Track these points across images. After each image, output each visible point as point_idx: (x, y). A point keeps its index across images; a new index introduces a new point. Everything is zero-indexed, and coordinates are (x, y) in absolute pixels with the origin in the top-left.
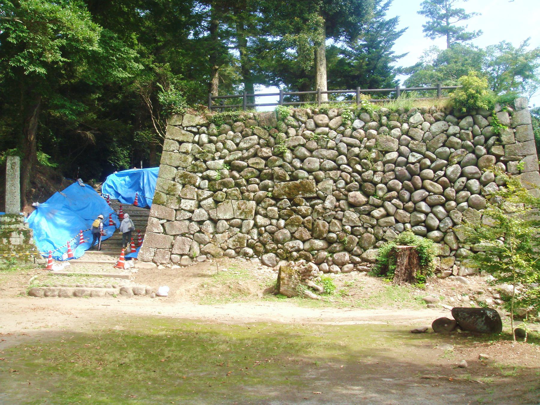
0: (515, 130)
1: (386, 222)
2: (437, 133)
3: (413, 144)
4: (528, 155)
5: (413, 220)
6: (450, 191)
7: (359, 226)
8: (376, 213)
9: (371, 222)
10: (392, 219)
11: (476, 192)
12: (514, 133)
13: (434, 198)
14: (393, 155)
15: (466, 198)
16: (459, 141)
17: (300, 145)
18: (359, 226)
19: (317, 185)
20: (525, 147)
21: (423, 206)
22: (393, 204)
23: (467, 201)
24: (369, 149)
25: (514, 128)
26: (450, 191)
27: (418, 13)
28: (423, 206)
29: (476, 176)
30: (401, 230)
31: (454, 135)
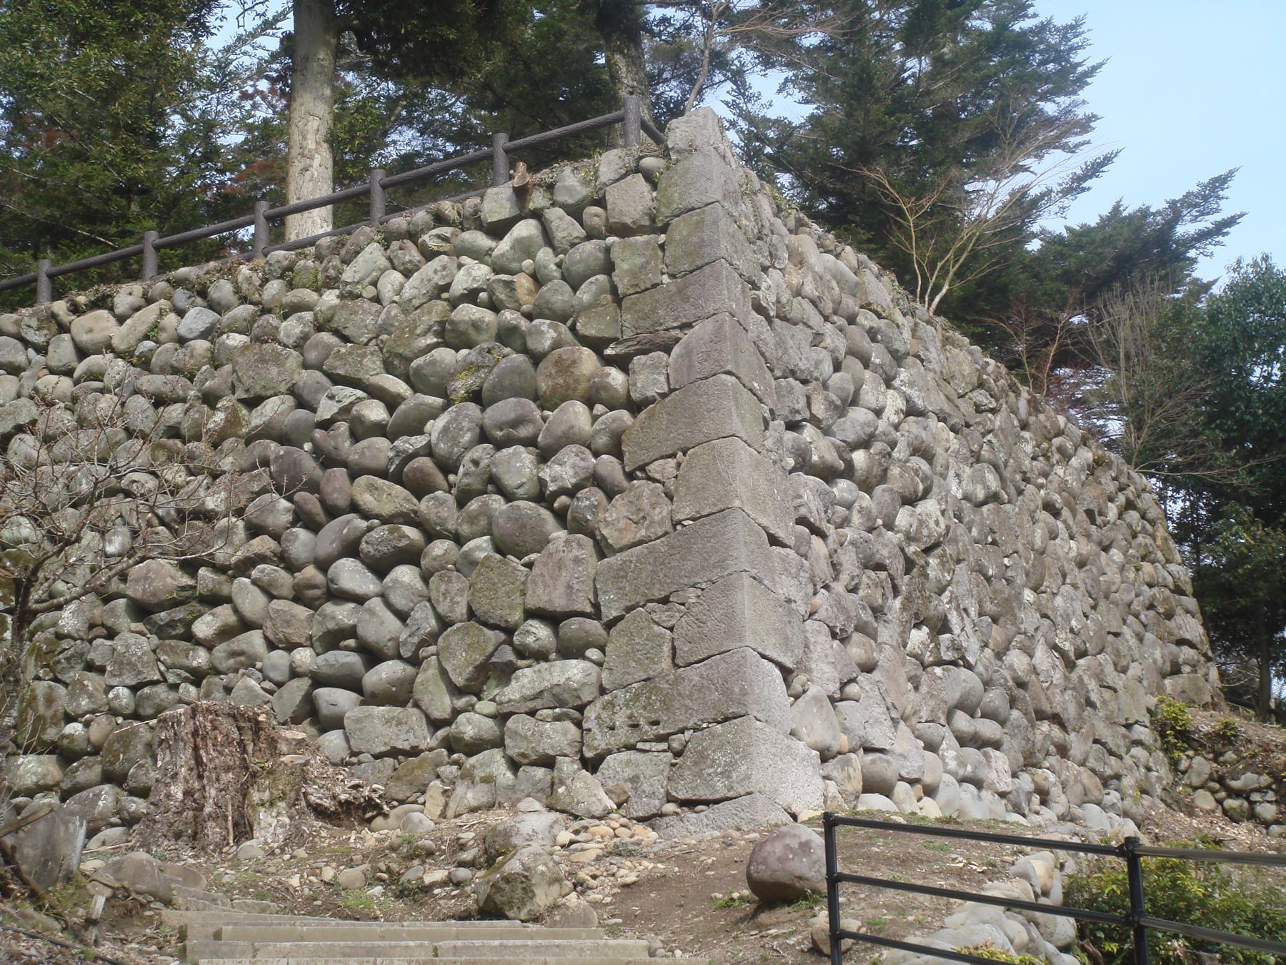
0: (662, 238)
1: (234, 654)
2: (416, 302)
3: (343, 358)
4: (699, 318)
5: (316, 631)
6: (440, 506)
7: (153, 683)
8: (205, 626)
9: (186, 662)
10: (254, 640)
11: (521, 491)
12: (662, 247)
13: (379, 539)
14: (274, 408)
15: (483, 522)
16: (488, 316)
17: (20, 429)
18: (153, 683)
19: (908, 400)
20: (689, 291)
21: (350, 574)
22: (254, 583)
23: (488, 531)
24: (210, 399)
25: (663, 230)
26: (440, 506)
27: (1118, 203)
28: (350, 574)
29: (524, 432)
30: (277, 676)
31: (471, 296)
